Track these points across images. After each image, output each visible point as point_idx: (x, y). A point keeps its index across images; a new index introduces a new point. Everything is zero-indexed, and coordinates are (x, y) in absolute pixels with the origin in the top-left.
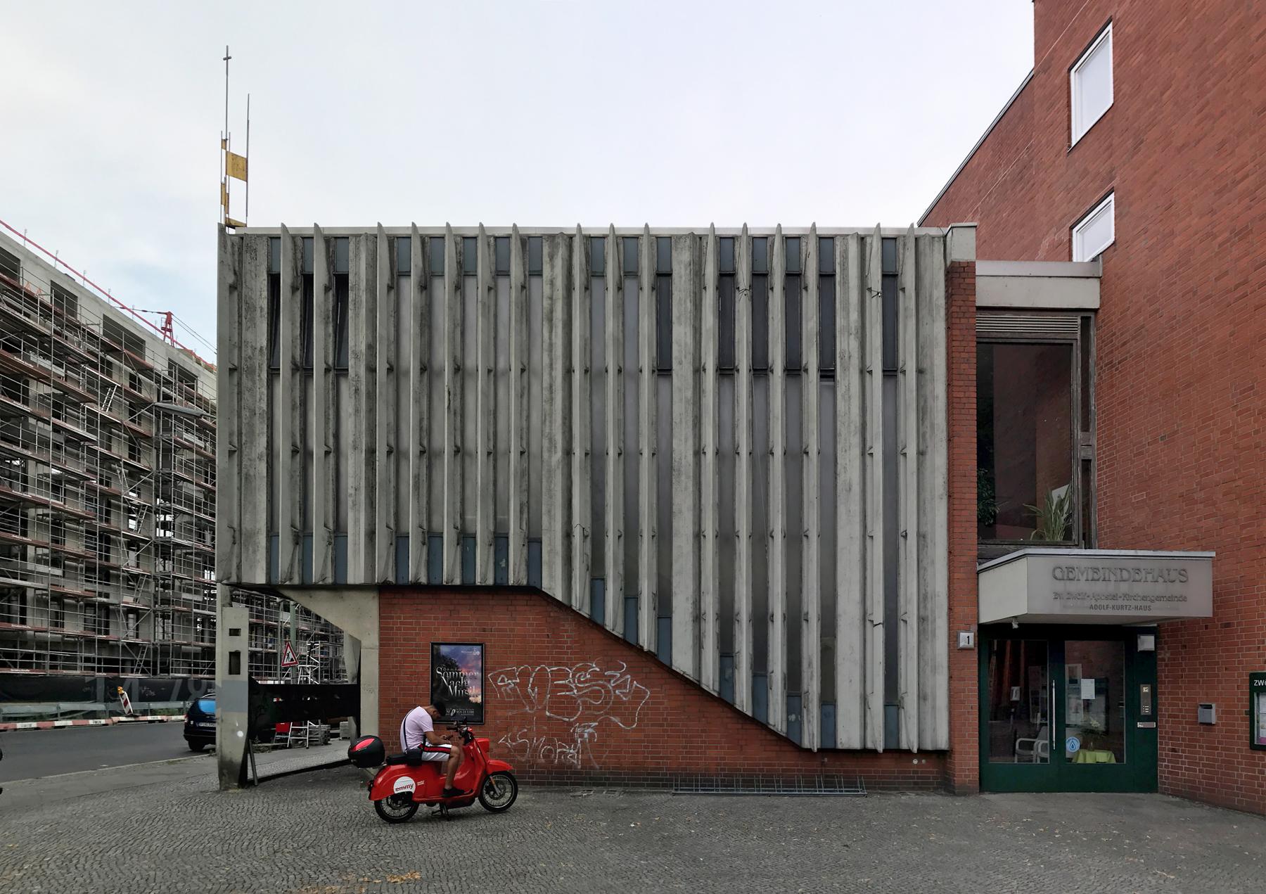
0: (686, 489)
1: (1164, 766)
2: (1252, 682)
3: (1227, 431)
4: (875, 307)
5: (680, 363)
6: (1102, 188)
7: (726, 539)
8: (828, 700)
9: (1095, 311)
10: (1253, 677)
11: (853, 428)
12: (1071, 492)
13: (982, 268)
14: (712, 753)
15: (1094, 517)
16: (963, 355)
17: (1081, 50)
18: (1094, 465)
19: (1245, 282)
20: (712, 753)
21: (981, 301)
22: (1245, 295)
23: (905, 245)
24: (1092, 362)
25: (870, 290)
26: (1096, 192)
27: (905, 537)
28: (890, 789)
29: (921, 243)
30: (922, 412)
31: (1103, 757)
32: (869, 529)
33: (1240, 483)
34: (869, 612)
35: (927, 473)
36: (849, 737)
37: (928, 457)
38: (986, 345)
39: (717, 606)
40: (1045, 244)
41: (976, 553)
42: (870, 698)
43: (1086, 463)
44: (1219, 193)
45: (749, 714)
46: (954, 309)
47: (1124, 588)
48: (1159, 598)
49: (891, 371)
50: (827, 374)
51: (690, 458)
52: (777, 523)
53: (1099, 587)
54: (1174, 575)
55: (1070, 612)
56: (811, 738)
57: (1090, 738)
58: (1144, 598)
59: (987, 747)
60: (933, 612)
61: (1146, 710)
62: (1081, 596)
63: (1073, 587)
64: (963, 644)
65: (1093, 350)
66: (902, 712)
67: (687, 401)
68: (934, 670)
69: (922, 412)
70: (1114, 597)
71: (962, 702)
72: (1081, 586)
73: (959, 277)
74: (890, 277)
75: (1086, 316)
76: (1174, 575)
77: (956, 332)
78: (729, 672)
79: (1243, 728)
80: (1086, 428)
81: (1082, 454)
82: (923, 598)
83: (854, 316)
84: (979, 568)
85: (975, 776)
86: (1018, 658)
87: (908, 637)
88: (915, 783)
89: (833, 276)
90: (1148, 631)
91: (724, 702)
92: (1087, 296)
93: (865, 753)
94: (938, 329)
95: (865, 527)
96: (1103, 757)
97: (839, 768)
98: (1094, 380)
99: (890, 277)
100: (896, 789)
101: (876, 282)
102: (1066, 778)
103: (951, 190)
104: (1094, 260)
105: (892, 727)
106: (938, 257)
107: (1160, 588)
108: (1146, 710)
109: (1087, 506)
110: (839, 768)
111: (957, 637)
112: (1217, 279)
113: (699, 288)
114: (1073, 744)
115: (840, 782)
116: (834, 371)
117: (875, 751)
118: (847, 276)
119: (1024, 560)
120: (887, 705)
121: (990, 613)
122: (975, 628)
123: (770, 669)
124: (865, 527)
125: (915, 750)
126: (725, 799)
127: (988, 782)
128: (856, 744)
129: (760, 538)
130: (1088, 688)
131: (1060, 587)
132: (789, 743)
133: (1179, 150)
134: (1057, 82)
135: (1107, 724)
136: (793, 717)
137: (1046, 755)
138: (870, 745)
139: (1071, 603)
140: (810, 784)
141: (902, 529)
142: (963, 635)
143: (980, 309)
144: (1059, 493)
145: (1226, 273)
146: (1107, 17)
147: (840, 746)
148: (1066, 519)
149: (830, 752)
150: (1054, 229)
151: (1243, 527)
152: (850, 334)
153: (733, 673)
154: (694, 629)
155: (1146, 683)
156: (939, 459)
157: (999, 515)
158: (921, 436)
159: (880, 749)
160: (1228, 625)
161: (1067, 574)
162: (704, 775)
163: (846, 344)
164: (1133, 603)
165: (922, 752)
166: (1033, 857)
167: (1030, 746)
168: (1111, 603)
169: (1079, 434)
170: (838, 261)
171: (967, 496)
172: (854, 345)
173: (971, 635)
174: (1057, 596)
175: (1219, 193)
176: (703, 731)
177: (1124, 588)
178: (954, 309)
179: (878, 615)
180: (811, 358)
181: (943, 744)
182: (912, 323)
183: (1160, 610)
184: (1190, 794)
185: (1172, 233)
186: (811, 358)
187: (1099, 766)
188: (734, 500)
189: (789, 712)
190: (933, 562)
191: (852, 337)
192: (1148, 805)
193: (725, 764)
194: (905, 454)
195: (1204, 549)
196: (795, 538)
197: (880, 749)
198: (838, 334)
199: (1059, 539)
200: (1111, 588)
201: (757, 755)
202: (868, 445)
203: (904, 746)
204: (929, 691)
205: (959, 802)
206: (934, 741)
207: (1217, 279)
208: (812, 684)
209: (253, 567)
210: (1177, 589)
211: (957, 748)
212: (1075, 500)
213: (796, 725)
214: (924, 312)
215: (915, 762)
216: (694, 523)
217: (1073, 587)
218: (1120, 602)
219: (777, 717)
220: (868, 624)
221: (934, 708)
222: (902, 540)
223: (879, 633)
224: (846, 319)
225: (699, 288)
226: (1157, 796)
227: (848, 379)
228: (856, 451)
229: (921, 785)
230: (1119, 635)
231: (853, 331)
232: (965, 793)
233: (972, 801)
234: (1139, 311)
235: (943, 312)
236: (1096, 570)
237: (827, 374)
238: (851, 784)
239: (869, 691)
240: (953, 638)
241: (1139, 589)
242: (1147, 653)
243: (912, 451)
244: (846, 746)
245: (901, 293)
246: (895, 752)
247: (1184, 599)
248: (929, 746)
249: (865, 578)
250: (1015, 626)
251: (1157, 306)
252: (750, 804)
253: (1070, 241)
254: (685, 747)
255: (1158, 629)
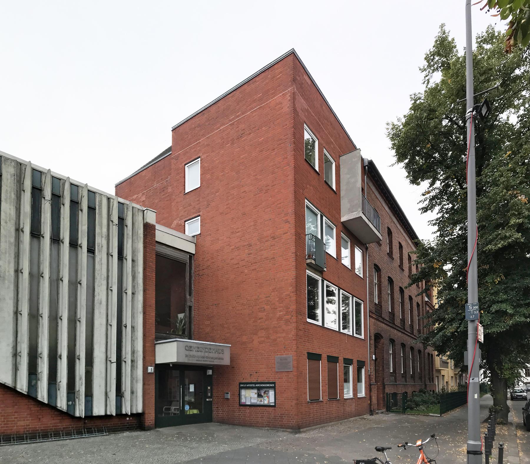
0: (8, 288)
1: (214, 413)
2: (275, 385)
3: (234, 307)
4: (115, 230)
5: (6, 223)
6: (196, 213)
7: (34, 317)
8: (89, 394)
9: (194, 254)
10: (240, 383)
11: (103, 277)
12: (185, 316)
13: (158, 227)
14: (22, 423)
15: (193, 327)
16: (150, 259)
17: (189, 161)
18: (193, 308)
19: (238, 264)
20: (22, 423)
21: (157, 239)
22: (238, 267)
23: (127, 208)
24: (193, 271)
25: (112, 221)
26: (194, 213)
27: (126, 327)
28: (117, 431)
29: (134, 210)
30: (134, 277)
31: (195, 411)
32: (109, 321)
33: (237, 324)
34: (109, 356)
35: (136, 302)
36: (98, 410)
37: (136, 295)
38: (159, 256)
39: (28, 350)
40: (175, 222)
41: (154, 337)
42: (109, 394)
43: (190, 307)
44: (232, 233)
45: (46, 401)
46: (147, 240)
47: (207, 354)
48: (216, 358)
49: (121, 257)
50: (91, 250)
51: (12, 273)
52: (64, 313)
53: (199, 354)
54: (220, 351)
55: (190, 362)
56: (80, 411)
57: (193, 406)
58: (212, 358)
59: (158, 410)
60: (137, 358)
61: (209, 394)
62: (194, 356)
63: (192, 353)
64: (149, 371)
65: (193, 268)
66: (123, 399)
67: (10, 243)
68: (137, 381)
69: (134, 277)
70: (203, 357)
71: (149, 394)
72: (194, 353)
73: (149, 229)
74: (121, 220)
75: (191, 255)
76: (220, 351)
77: (148, 250)
78: (34, 382)
79: (237, 399)
80: (190, 295)
81: (188, 304)
82: (133, 352)
83: (105, 230)
84: (156, 343)
85: (153, 422)
86: (164, 378)
87: (127, 369)
88: (128, 428)
89: (95, 209)
90: (210, 368)
91: (31, 397)
92: (191, 248)
93: (107, 417)
94: (140, 246)
95: (107, 320)
96: (195, 411)
97: (92, 425)
98: (193, 278)
99: (121, 220)
100: (119, 431)
101: (116, 220)
102: (183, 420)
103: (132, 179)
104: (193, 237)
105: (119, 406)
106: (141, 218)
107: (216, 355)
108: (209, 394)
109: (190, 322)
110: (92, 425)
111: (147, 368)
112: (231, 259)
113: (20, 190)
114: (187, 407)
115: (95, 431)
116: (94, 250)
117: (111, 416)
118: (102, 212)
119: (176, 343)
120: (86, 396)
121: (159, 360)
122: (154, 365)
123: (58, 381)
124: (107, 320)
125: (129, 414)
126: (33, 445)
127: (159, 423)
128: (102, 413)
129: (54, 319)
130: (192, 388)
131: (187, 353)
132: (68, 415)
133: (221, 213)
134: (181, 166)
135: (240, 395)
136: (70, 403)
137: (177, 412)
138: (108, 413)
139: (191, 359)
140: (80, 433)
141: (124, 323)
142: (150, 368)
143: (157, 242)
144: (181, 316)
145: (233, 259)
146: (199, 156)
147: (94, 415)
148: (183, 326)
149: (90, 417)
150: (178, 219)
151: (237, 338)
152: (102, 237)
153: (36, 383)
154: (13, 361)
155: (209, 386)
156: (140, 297)
157: (164, 322)
158: (133, 287)
159: (114, 414)
160: (233, 367)
161: (189, 348)
162: (16, 435)
163: (100, 241)
164: (209, 360)
165: (132, 415)
166: (185, 447)
167: (169, 409)
168: (203, 359)
169: (188, 297)
170: (97, 204)
171: (151, 314)
172: (104, 242)
173: (153, 368)
174: (186, 356)
175: (232, 233)
176: (15, 412)
177: (207, 354)
178: (147, 240)
179: (114, 359)
180: (83, 241)
181: (140, 410)
182: (130, 241)
183: (216, 362)
184: (223, 422)
185: (218, 239)
186: (83, 241)
187: (194, 415)
188: (38, 298)
189: (68, 401)
190: (137, 338)
191: (103, 239)
192: (212, 427)
193: (29, 428)
194: (126, 293)
195: (227, 343)
196: (73, 321)
197: (114, 414)
198: (96, 235)
199: (180, 333)
200: (202, 354)
201: (49, 421)
202: (110, 285)
203: (124, 412)
204: (135, 390)
205: (148, 433)
206: (137, 410)
207: (231, 259)
208: (81, 386)
209: (361, 392)
210: (221, 356)
211: (146, 412)
212: (186, 320)
213: (72, 406)
214: (135, 238)
215: (128, 419)
216: (14, 307)
217: (192, 353)
218: (205, 359)
219: (62, 403)
220: (109, 362)
221: (137, 396)
222: (124, 328)
223: (114, 366)
224: (101, 230)
225: (20, 190)
226: (212, 423)
227: (101, 256)
228: (104, 287)
229: (130, 428)
230: (201, 369)
231: (104, 236)
232: (148, 429)
233: (152, 432)
234: (208, 260)
235: (142, 240)
236: (198, 348)
237: (91, 250)
238: (100, 431)
239: (108, 390)
240: (145, 369)
241: (211, 355)
242: (210, 375)
243: (129, 292)
244: (97, 414)
245: (125, 227)
246: (120, 415)
247: (223, 359)
248: (134, 412)
249: (107, 342)
250: (171, 365)
251: (213, 261)
252: (49, 445)
253: (184, 226)
254: (4, 421)
255: (213, 367)
